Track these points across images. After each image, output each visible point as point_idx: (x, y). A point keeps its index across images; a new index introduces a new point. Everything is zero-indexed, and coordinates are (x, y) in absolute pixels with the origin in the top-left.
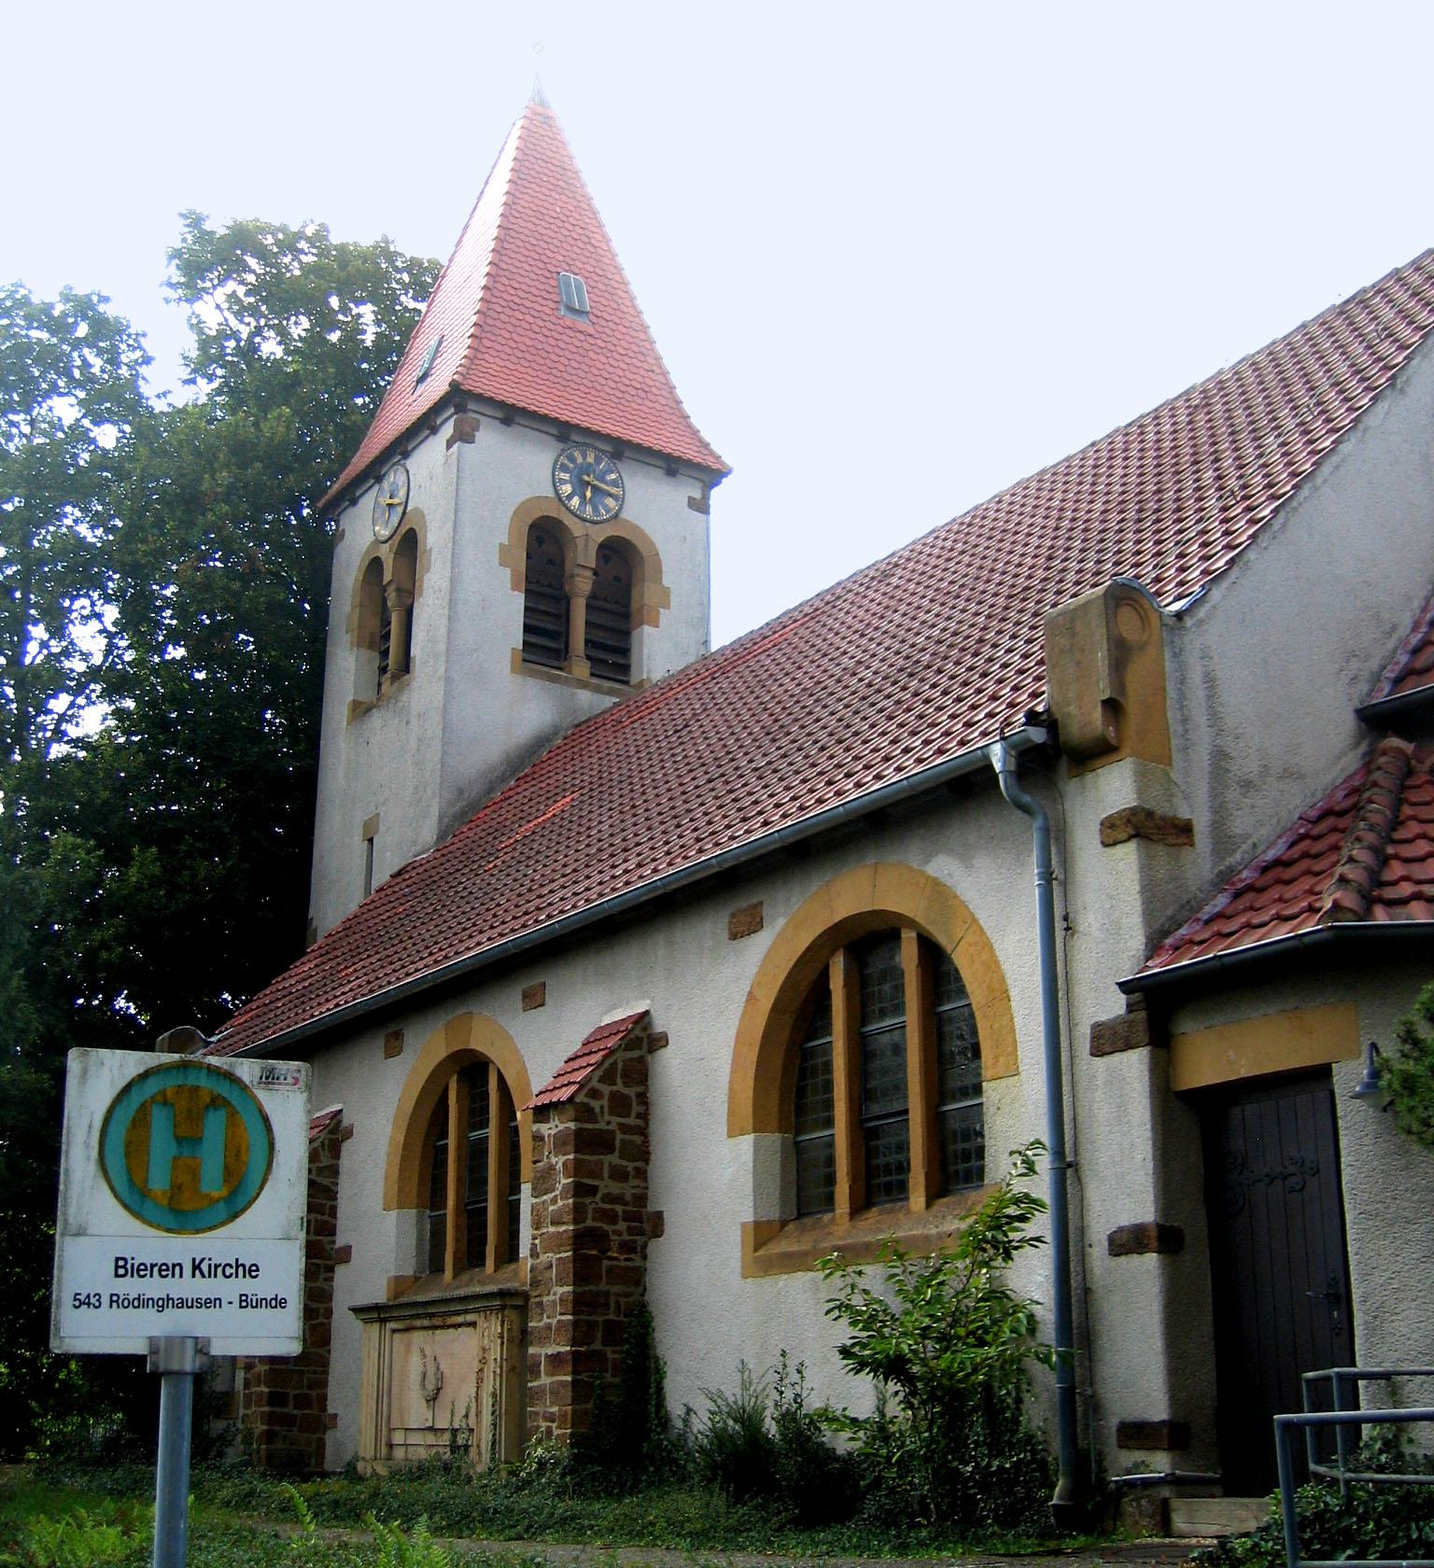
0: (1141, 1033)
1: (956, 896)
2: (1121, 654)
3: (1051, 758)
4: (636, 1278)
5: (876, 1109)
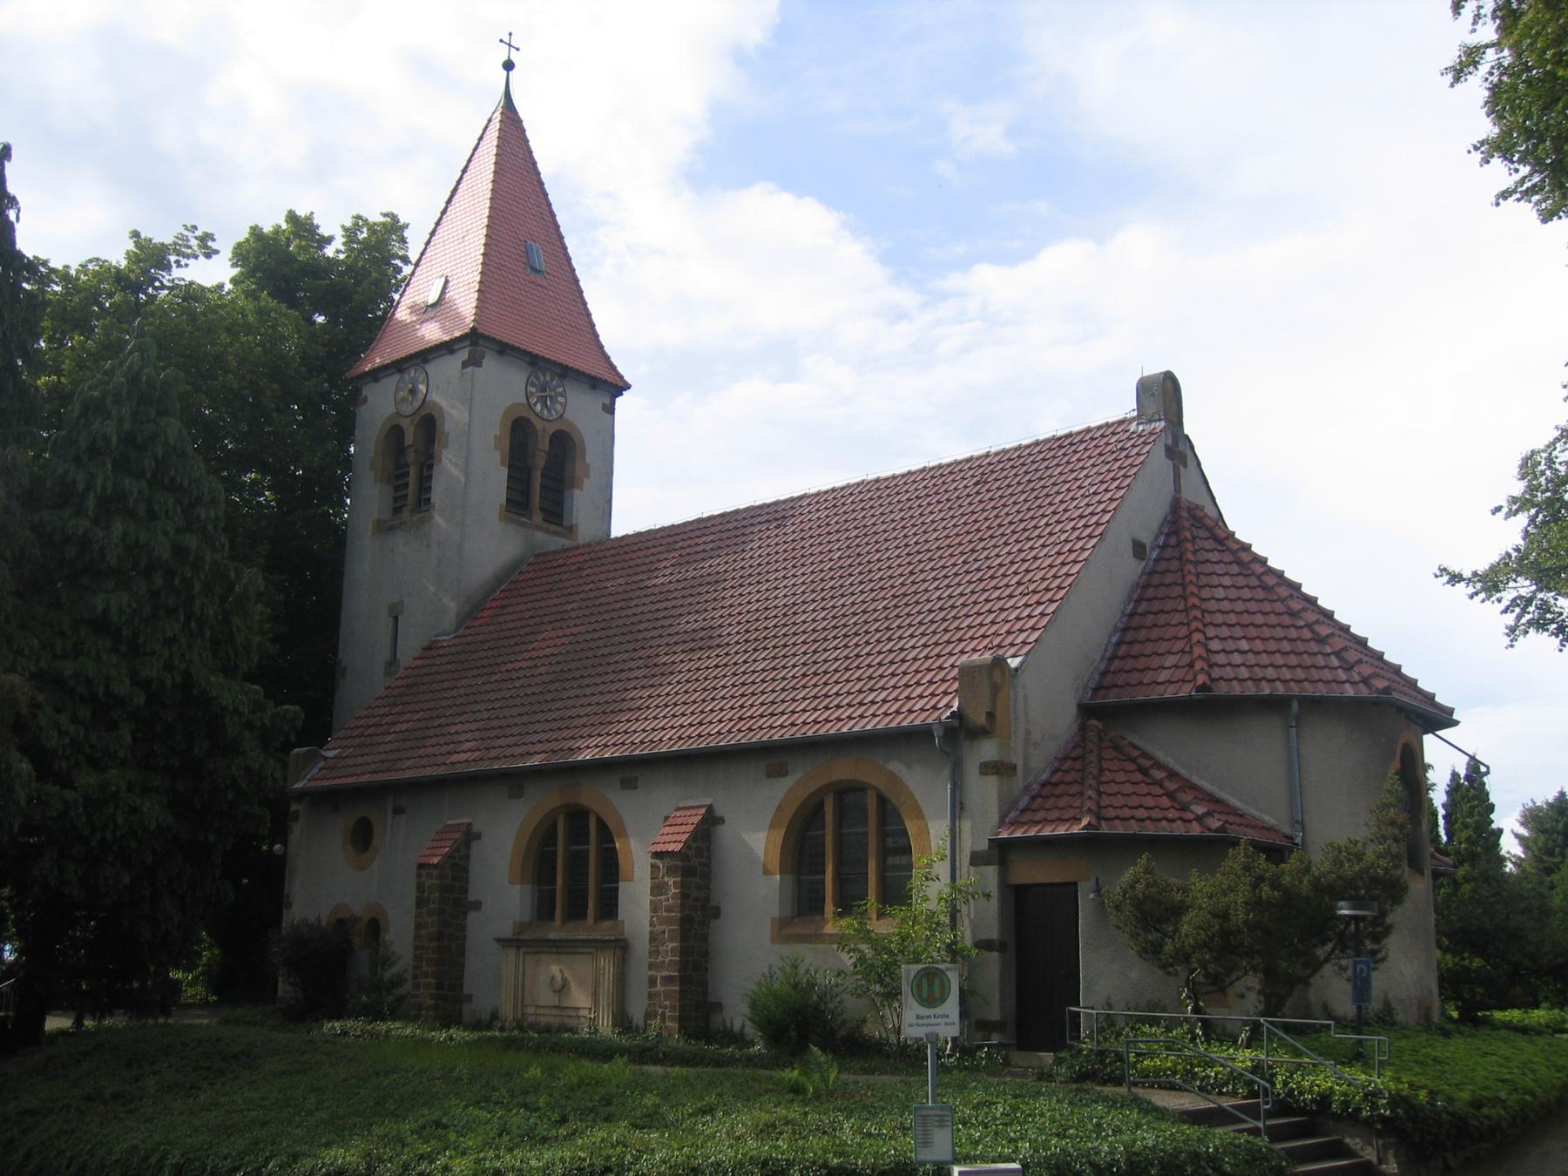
2: (995, 690)
3: (961, 730)
4: (704, 938)
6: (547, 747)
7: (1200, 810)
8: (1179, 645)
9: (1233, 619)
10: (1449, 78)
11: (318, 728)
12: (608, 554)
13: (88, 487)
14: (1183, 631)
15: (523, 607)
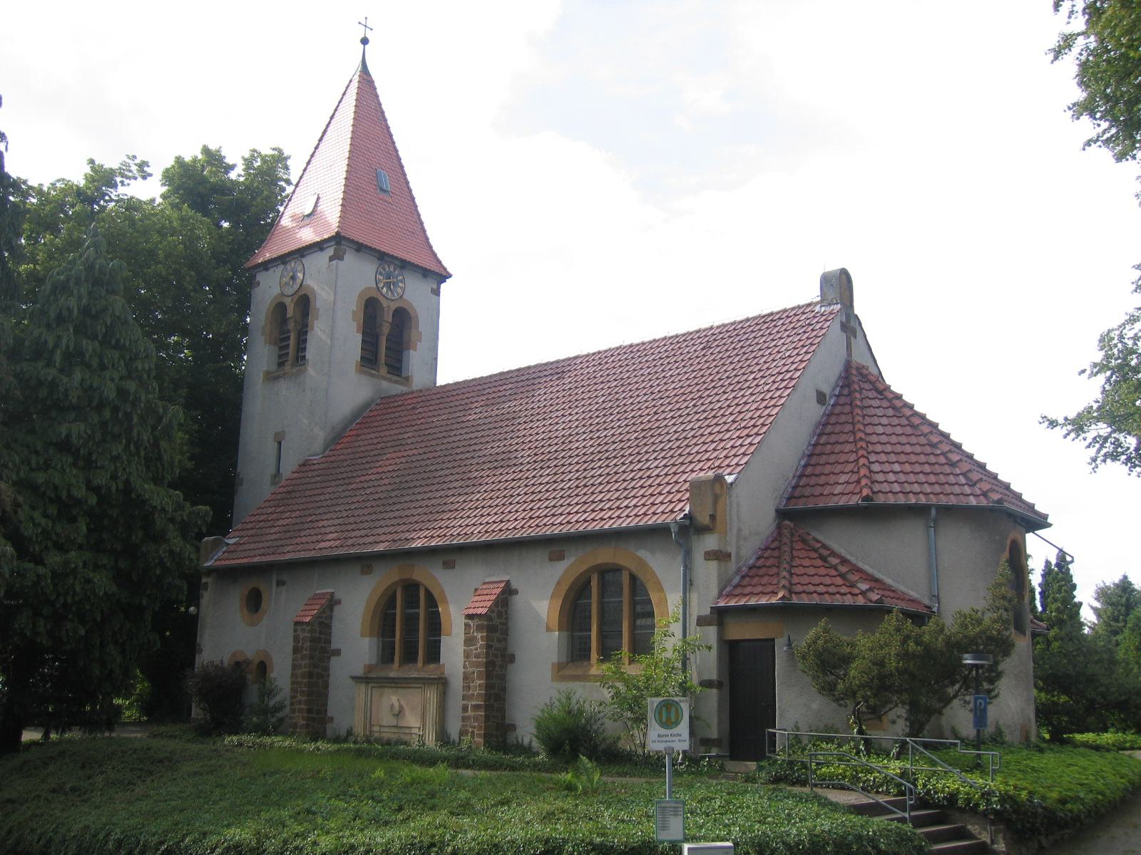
1: (648, 565)
3: (690, 528)
4: (503, 678)
8: (850, 467)
10: (1051, 56)
11: (222, 524)
13: (56, 346)
14: (853, 457)
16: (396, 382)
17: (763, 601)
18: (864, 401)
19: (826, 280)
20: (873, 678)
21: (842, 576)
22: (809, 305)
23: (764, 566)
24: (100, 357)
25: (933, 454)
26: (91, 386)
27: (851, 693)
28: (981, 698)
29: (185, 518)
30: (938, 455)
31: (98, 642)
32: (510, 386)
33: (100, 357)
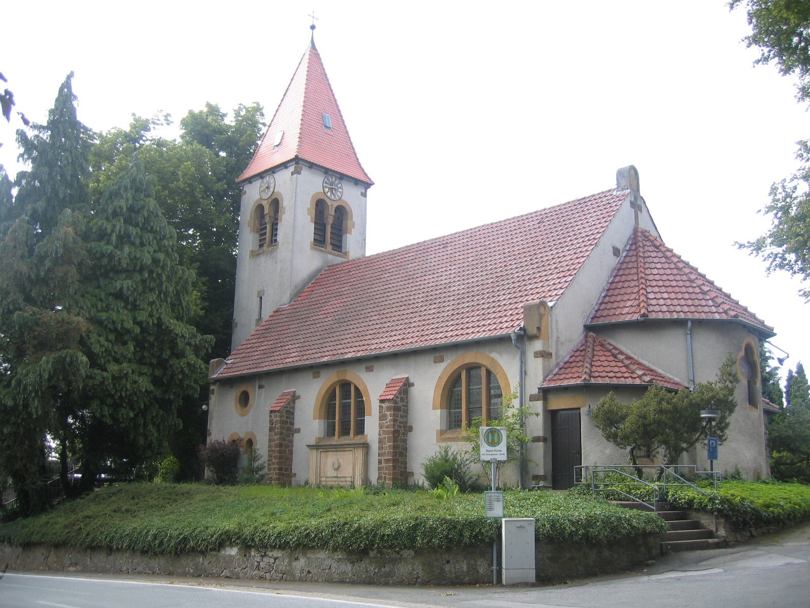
0: (541, 397)
3: (524, 337)
4: (405, 441)
5: (472, 406)
6: (331, 353)
7: (640, 372)
8: (633, 296)
9: (661, 283)
10: (728, 8)
11: (223, 348)
12: (363, 264)
13: (113, 231)
14: (636, 290)
15: (322, 290)
16: (338, 256)
17: (572, 382)
18: (645, 253)
19: (620, 174)
20: (640, 427)
21: (626, 366)
22: (610, 191)
23: (575, 361)
24: (141, 238)
25: (691, 286)
26: (135, 257)
27: (625, 438)
28: (713, 440)
29: (198, 342)
30: (695, 287)
31: (142, 423)
32: (412, 254)
33: (141, 238)
